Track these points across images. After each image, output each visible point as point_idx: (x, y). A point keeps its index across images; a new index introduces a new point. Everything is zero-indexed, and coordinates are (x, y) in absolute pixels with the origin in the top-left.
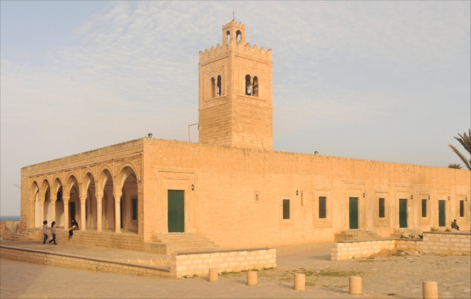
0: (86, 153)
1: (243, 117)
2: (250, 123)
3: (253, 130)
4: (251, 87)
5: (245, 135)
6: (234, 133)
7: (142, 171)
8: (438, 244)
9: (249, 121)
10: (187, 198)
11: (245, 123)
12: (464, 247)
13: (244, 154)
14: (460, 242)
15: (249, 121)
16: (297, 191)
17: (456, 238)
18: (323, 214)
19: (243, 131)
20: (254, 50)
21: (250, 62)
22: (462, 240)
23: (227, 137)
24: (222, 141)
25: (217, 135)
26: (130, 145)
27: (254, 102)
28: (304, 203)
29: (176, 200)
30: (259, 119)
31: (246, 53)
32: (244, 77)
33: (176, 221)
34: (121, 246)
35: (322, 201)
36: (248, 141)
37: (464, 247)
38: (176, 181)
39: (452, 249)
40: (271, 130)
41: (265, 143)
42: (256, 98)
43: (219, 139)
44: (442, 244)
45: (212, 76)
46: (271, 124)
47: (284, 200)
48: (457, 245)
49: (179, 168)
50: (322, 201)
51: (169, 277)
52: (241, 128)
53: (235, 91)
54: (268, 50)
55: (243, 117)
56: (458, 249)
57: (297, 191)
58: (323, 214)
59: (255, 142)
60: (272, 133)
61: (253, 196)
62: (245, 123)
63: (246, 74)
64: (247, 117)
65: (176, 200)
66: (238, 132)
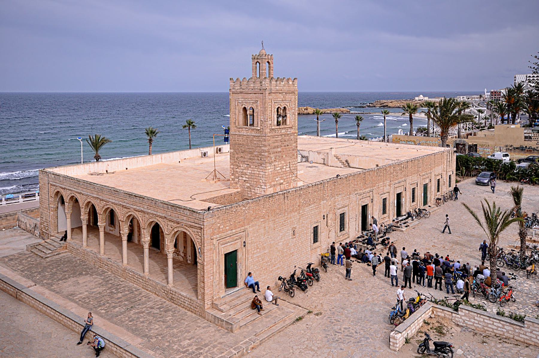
0: (130, 195)
2: (280, 152)
3: (282, 157)
7: (202, 243)
8: (473, 320)
9: (279, 150)
10: (239, 255)
12: (496, 329)
14: (493, 324)
15: (279, 150)
16: (324, 216)
17: (489, 320)
18: (315, 240)
21: (281, 95)
22: (495, 324)
25: (250, 162)
26: (188, 213)
28: (329, 224)
29: (231, 260)
30: (288, 146)
34: (175, 302)
35: (342, 216)
37: (496, 329)
38: (231, 243)
39: (485, 328)
42: (285, 126)
44: (477, 322)
45: (244, 106)
48: (490, 326)
49: (234, 231)
50: (342, 216)
52: (273, 159)
53: (269, 125)
54: (294, 80)
55: (275, 148)
56: (491, 330)
57: (324, 216)
58: (315, 240)
65: (231, 260)
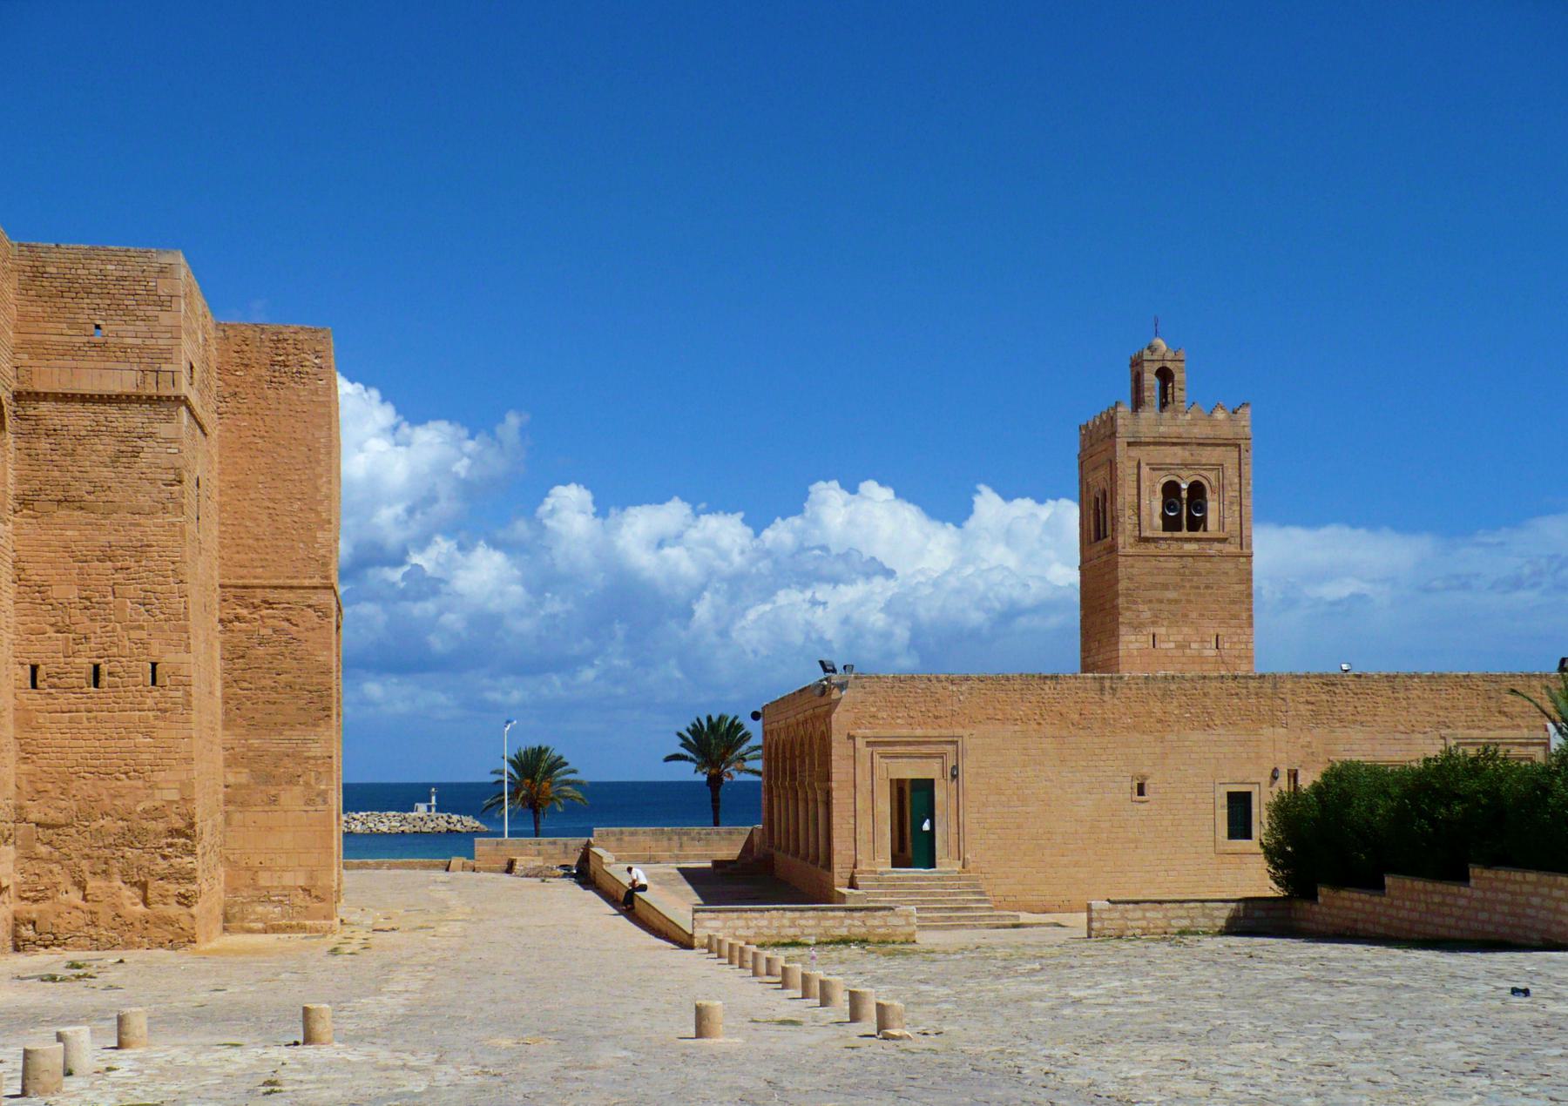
1: (1154, 586)
2: (1176, 601)
4: (49, 893)
5: (1161, 631)
6: (1123, 630)
9: (1172, 595)
11: (1161, 601)
13: (1102, 689)
15: (1172, 595)
19: (1153, 623)
20: (1188, 417)
27: (1191, 547)
30: (1207, 587)
31: (1162, 429)
32: (1159, 488)
33: (913, 846)
36: (1172, 645)
40: (1250, 610)
41: (1227, 645)
46: (1250, 595)
47: (933, 866)
51: (915, 952)
52: (1148, 614)
55: (1154, 586)
59: (1194, 646)
60: (1251, 616)
61: (1129, 786)
62: (1161, 601)
63: (1164, 480)
64: (1165, 587)
66: (1137, 627)
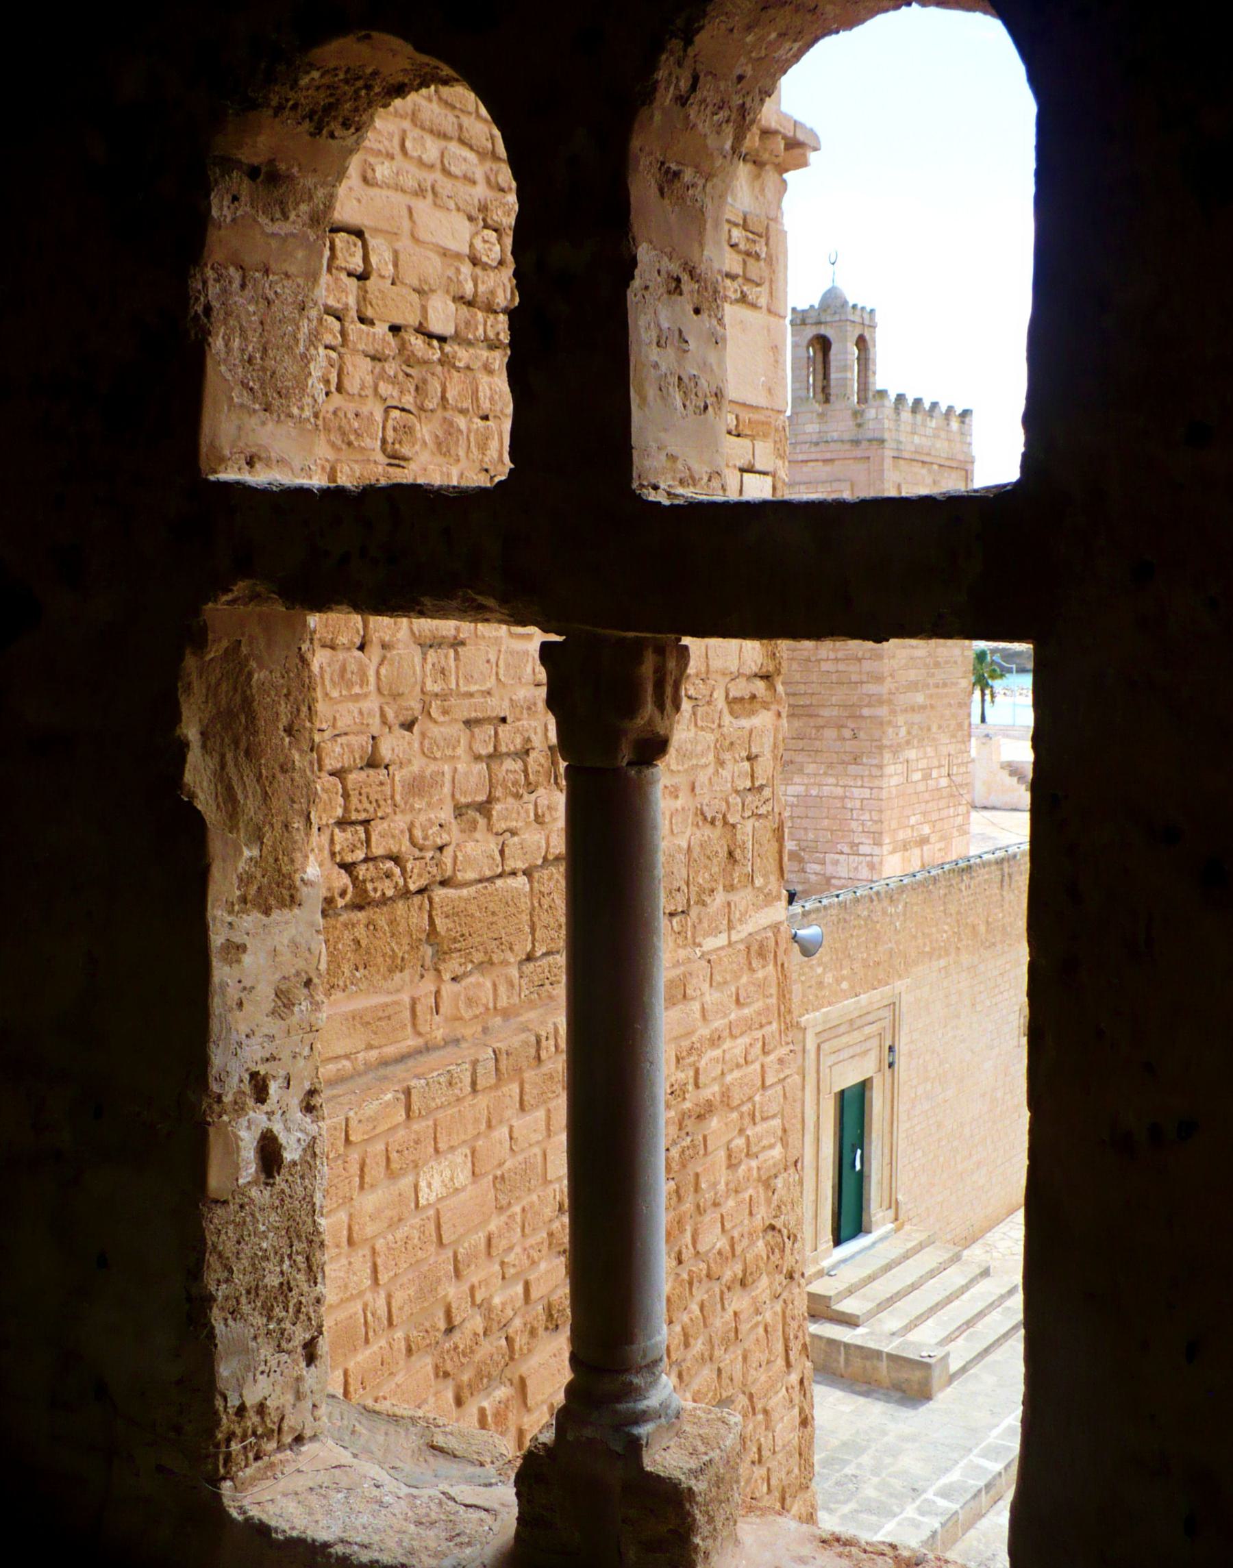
2: (923, 707)
9: (920, 698)
15: (920, 698)
23: (852, 769)
24: (832, 780)
43: (811, 768)
